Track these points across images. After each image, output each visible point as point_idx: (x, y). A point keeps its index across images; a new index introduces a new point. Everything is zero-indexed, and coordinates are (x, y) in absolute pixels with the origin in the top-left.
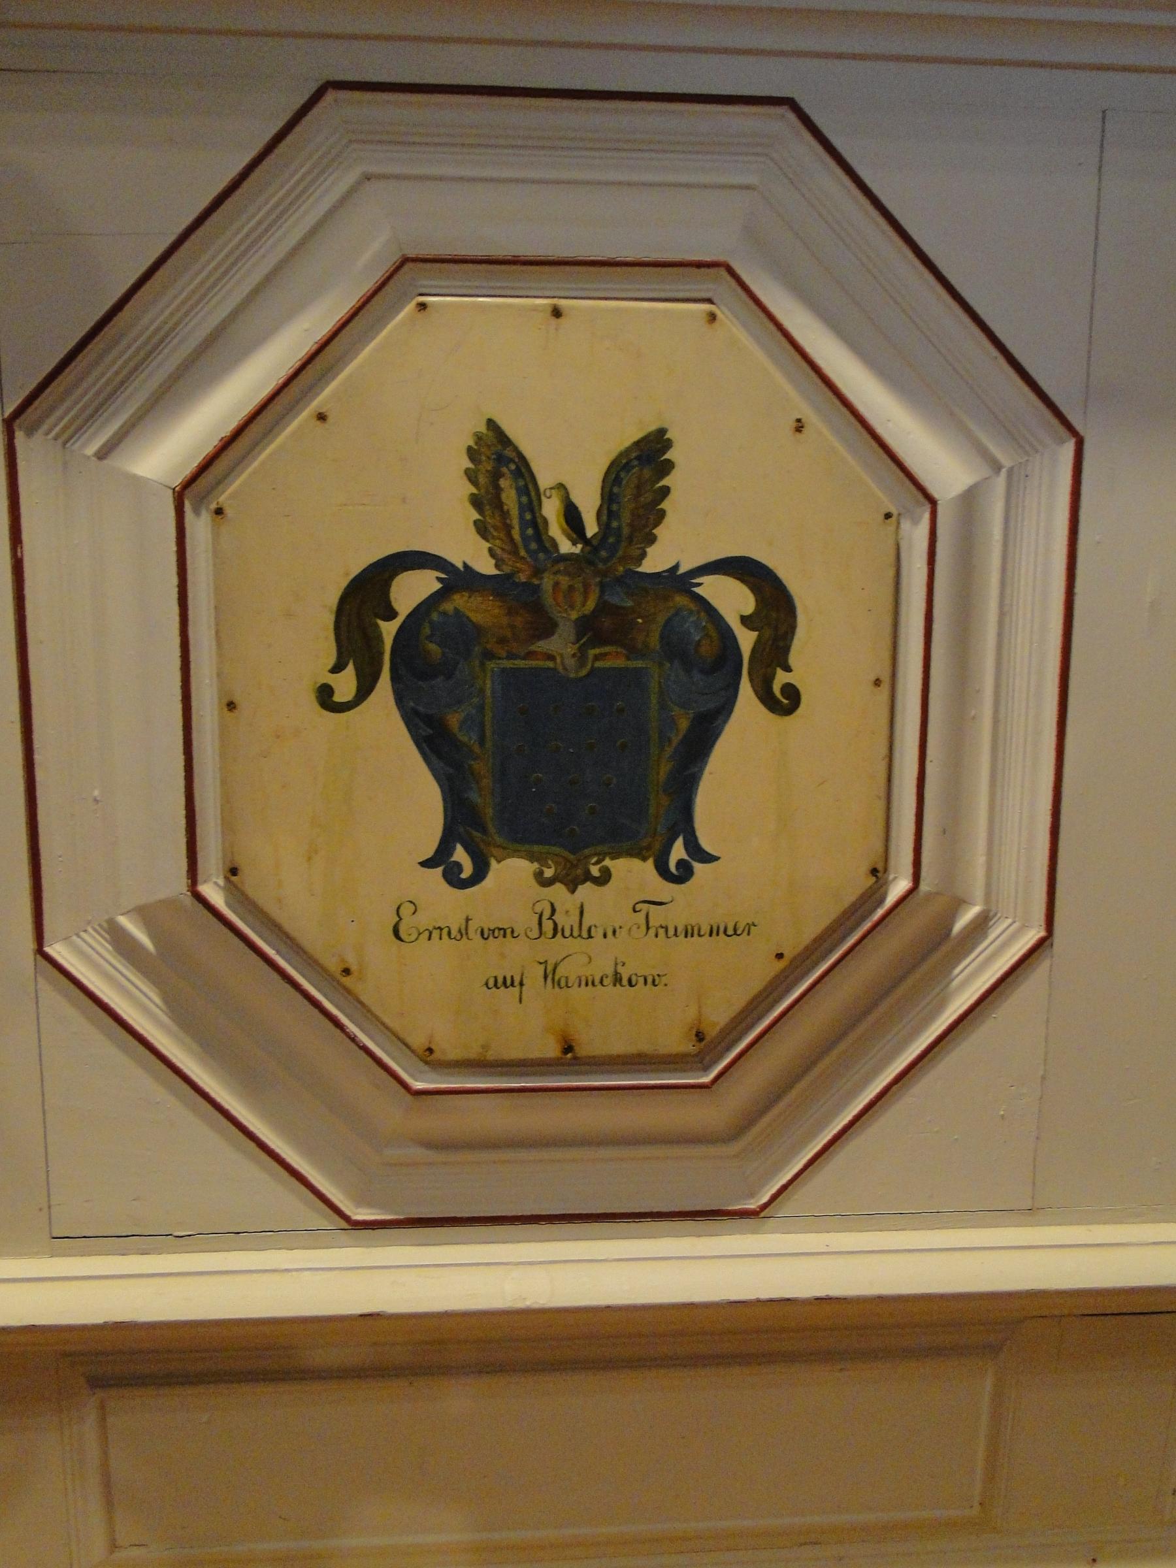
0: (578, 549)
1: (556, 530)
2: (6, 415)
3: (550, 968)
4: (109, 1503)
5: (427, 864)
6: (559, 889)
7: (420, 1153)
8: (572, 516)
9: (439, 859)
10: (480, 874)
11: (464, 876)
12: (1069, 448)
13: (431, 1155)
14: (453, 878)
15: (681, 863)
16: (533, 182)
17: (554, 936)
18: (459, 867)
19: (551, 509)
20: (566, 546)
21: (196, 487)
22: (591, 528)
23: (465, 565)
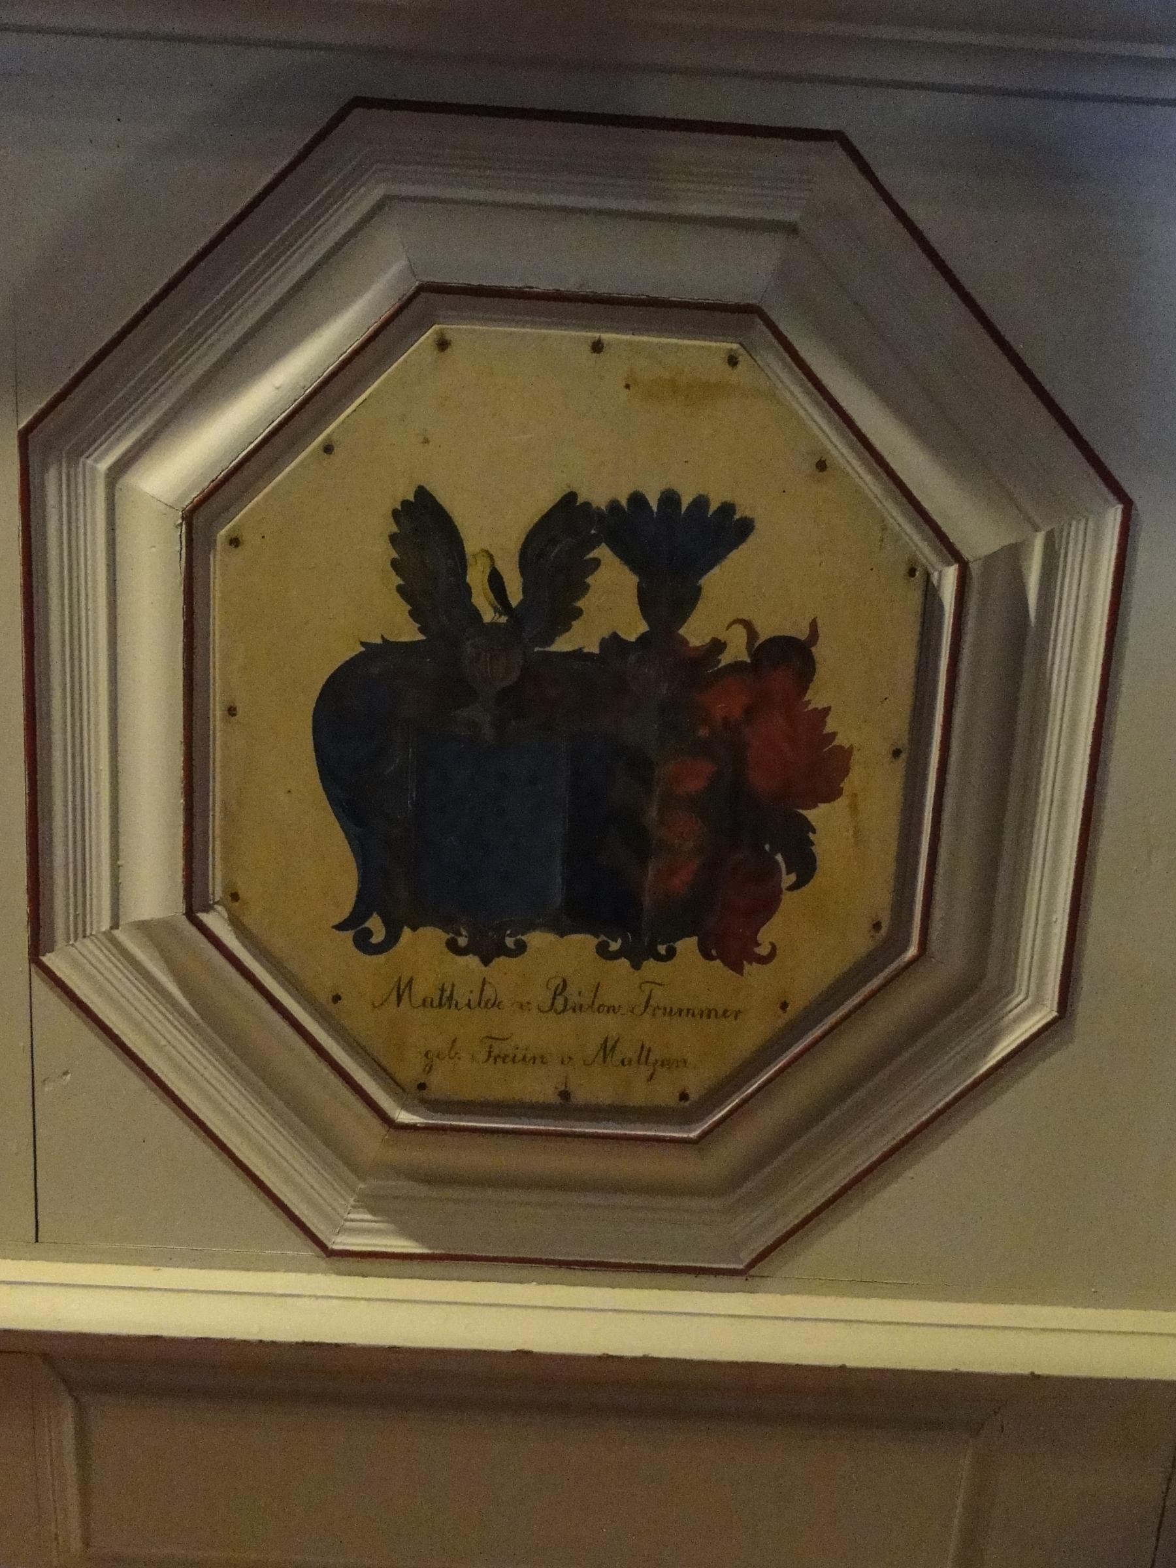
0: (503, 619)
1: (482, 600)
2: (21, 426)
3: (610, 1044)
4: (70, 1391)
5: (341, 927)
6: (473, 961)
7: (408, 1187)
8: (496, 581)
9: (353, 922)
10: (392, 938)
11: (375, 940)
12: (1114, 516)
13: (423, 1190)
14: (363, 943)
15: (668, 950)
16: (749, 75)
17: (564, 1011)
18: (369, 933)
19: (477, 578)
20: (488, 615)
21: (202, 518)
22: (515, 596)
23: (579, 613)
